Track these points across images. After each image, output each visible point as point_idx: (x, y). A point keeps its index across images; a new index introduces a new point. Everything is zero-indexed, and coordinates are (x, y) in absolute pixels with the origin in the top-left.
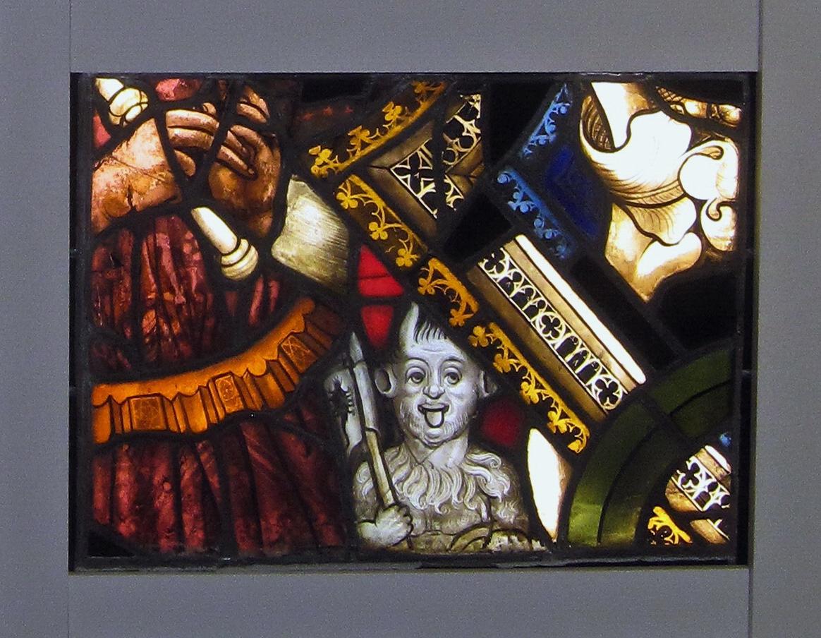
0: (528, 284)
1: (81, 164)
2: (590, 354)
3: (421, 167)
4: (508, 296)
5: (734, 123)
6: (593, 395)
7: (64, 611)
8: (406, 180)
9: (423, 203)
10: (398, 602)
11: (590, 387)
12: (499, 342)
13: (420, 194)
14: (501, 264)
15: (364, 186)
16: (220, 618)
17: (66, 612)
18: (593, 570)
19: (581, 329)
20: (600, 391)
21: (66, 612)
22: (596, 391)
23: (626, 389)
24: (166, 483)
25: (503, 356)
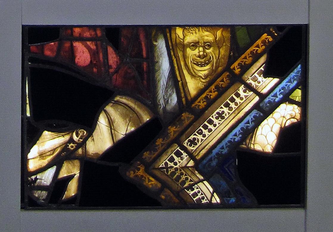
0: (229, 114)
1: (25, 146)
2: (236, 107)
3: (165, 170)
4: (167, 160)
5: (32, 194)
6: (191, 137)
7: (20, 6)
8: (163, 165)
9: (170, 157)
10: (161, 3)
11: (222, 108)
12: (252, 52)
13: (174, 154)
14: (165, 165)
15: (199, 99)
16: (86, 9)
17: (21, 6)
18: (121, 211)
19: (238, 110)
20: (220, 112)
21: (21, 6)
22: (220, 111)
23: (260, 86)
24: (130, 172)
25: (211, 95)
